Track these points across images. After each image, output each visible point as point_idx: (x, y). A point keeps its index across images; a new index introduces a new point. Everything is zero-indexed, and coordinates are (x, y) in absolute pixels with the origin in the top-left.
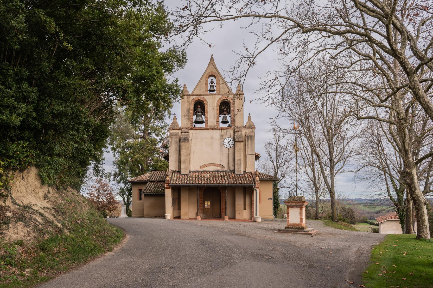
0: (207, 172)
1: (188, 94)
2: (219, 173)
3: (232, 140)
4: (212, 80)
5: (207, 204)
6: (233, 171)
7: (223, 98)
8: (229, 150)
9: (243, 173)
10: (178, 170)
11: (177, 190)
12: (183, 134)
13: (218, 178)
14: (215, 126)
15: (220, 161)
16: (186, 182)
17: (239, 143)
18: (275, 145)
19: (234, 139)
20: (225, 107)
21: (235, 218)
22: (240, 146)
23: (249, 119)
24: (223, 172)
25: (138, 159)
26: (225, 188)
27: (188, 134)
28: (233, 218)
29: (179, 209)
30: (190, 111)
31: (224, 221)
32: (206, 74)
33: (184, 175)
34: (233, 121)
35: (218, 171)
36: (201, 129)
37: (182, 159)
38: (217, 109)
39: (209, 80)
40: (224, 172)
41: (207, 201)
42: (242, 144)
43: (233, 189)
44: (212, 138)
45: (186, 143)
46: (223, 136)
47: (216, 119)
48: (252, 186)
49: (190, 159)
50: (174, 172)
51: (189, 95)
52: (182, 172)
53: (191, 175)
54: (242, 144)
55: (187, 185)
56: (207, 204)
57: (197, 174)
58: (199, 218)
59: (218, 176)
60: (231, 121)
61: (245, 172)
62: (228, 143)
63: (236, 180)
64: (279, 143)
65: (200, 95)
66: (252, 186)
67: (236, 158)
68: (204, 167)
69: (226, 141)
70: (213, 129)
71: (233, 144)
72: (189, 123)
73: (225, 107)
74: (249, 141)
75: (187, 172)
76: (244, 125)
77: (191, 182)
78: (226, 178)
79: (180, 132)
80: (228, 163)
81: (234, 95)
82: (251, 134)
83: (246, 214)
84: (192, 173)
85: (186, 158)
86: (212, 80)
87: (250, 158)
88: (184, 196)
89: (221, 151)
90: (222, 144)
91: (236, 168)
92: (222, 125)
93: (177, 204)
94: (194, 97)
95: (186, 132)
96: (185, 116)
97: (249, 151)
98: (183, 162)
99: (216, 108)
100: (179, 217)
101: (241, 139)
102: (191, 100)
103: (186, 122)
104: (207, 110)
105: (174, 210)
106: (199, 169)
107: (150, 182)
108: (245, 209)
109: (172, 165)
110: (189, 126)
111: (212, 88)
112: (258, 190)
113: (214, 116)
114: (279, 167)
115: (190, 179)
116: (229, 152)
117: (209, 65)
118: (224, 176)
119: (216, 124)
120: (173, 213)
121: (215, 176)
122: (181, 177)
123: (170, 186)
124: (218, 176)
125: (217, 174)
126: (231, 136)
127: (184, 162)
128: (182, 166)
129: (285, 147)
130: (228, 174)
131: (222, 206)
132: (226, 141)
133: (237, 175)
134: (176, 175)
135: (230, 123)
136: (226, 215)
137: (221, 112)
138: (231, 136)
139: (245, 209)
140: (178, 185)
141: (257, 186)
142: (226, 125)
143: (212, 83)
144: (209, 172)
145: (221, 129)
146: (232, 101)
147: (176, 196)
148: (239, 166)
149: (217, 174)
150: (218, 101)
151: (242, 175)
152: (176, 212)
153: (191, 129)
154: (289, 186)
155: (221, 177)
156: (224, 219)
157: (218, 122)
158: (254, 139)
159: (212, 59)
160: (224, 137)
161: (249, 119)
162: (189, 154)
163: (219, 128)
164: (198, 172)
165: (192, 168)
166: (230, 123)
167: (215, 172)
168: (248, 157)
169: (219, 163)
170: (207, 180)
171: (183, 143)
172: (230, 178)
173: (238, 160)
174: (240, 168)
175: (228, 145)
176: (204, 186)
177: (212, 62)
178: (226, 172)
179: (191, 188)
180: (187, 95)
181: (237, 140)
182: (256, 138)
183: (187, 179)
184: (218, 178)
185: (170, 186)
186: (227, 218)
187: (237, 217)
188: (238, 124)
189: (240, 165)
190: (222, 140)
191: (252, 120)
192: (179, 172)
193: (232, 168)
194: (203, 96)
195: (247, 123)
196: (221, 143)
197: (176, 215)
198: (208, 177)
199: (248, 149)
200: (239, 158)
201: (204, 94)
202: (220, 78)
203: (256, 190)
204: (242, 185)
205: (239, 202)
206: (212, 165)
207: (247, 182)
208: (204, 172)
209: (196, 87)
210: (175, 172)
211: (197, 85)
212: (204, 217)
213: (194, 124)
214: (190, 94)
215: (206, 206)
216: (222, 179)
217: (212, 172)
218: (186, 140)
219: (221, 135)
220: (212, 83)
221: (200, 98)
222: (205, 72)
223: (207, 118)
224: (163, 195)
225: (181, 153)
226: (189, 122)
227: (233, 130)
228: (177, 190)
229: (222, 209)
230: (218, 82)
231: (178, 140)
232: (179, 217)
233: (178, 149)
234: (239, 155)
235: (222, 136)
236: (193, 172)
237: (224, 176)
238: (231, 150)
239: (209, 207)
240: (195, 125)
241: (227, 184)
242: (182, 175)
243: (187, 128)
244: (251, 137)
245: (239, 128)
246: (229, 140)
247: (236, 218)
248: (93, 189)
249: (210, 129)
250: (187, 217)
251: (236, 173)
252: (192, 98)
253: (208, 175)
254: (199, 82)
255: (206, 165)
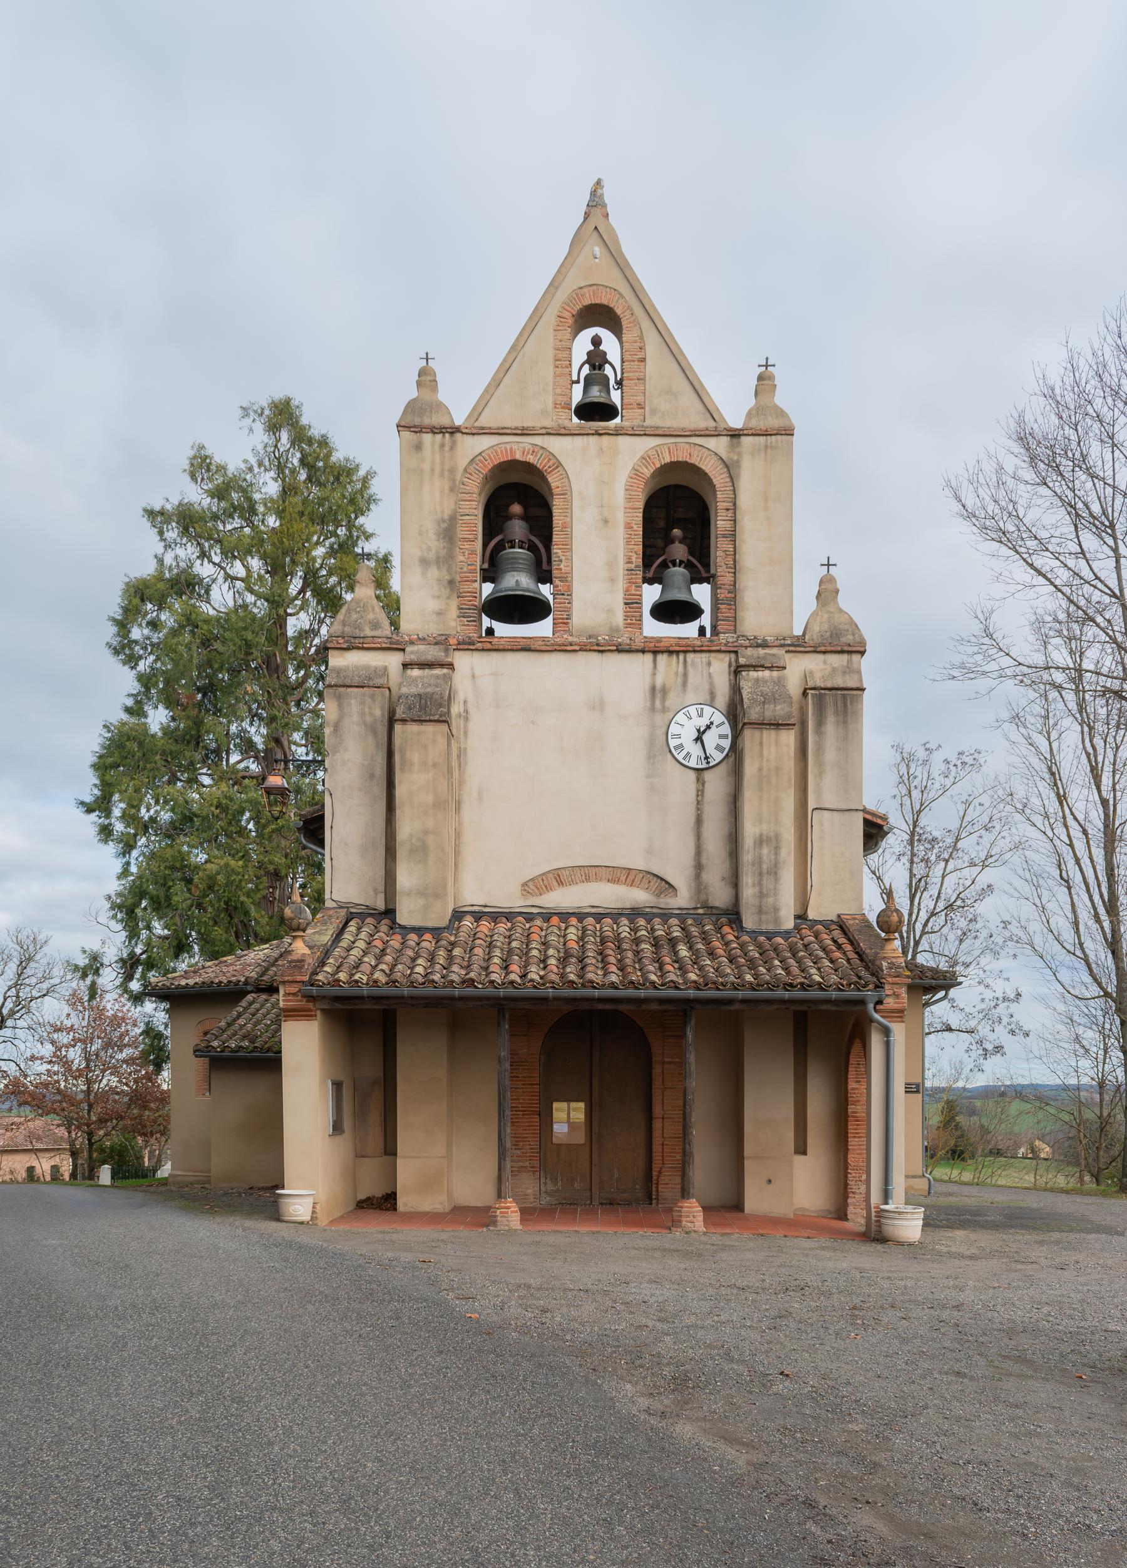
0: (564, 916)
1: (445, 422)
2: (641, 922)
3: (719, 718)
4: (596, 341)
5: (568, 1118)
6: (726, 912)
7: (668, 452)
8: (700, 781)
9: (789, 924)
10: (381, 905)
11: (370, 1026)
12: (416, 673)
13: (637, 953)
14: (614, 630)
15: (650, 852)
16: (420, 970)
17: (769, 735)
18: (905, 827)
19: (735, 714)
20: (680, 520)
21: (737, 1206)
22: (770, 752)
23: (827, 592)
24: (665, 916)
25: (221, 879)
26: (677, 1012)
27: (448, 679)
28: (729, 1206)
29: (390, 1150)
30: (461, 532)
31: (677, 1234)
32: (561, 296)
33: (419, 931)
34: (728, 603)
35: (634, 913)
36: (525, 647)
37: (406, 828)
38: (628, 526)
39: (582, 345)
40: (674, 921)
41: (569, 1100)
42: (789, 738)
43: (726, 1021)
44: (598, 705)
45: (429, 728)
46: (664, 691)
47: (621, 585)
48: (862, 1002)
49: (458, 834)
50: (352, 915)
51: (454, 430)
52: (404, 917)
53: (463, 936)
54: (789, 738)
55: (429, 990)
56: (568, 1118)
57: (502, 927)
58: (510, 1215)
59: (637, 941)
60: (715, 609)
61: (801, 917)
62: (699, 739)
63: (752, 965)
64: (922, 822)
65: (524, 432)
66: (862, 1002)
67: (750, 830)
68: (549, 888)
69: (684, 729)
70: (600, 649)
71: (726, 744)
72: (454, 612)
73: (680, 520)
74: (830, 727)
75: (439, 917)
76: (798, 631)
77: (457, 973)
78: (683, 951)
79: (392, 661)
80: (699, 867)
81: (735, 435)
82: (839, 682)
83: (805, 1184)
84: (468, 922)
85: (430, 823)
86: (596, 341)
87: (835, 837)
88: (420, 1065)
89: (652, 789)
90: (660, 747)
91: (748, 892)
92: (654, 629)
93: (375, 1117)
94: (486, 442)
95: (429, 665)
96: (424, 562)
97: (825, 789)
98: (413, 851)
99: (620, 517)
100: (386, 1202)
101: (778, 710)
102: (462, 462)
103: (433, 605)
104: (567, 527)
105: (359, 1155)
106: (514, 901)
107: (259, 990)
108: (801, 1149)
109: (347, 875)
110: (454, 625)
111: (596, 394)
112: (898, 1031)
113: (611, 565)
114: (923, 933)
115: (450, 958)
116: (700, 792)
117: (577, 241)
118: (673, 942)
119: (619, 619)
120: (352, 1177)
121: (618, 940)
122: (395, 943)
123: (310, 998)
124: (637, 941)
125: (625, 931)
126: (712, 695)
127: (420, 850)
128: (405, 878)
129: (949, 840)
130: (694, 931)
131: (657, 1134)
132: (684, 729)
133: (754, 934)
134: (366, 929)
135: (706, 620)
136: (685, 1193)
137: (653, 562)
138: (712, 695)
139: (801, 1149)
140: (365, 991)
141: (890, 1003)
142: (688, 630)
143: (597, 360)
144: (581, 917)
145: (655, 649)
146: (719, 478)
147: (372, 1068)
148: (768, 882)
149: (625, 931)
150: (636, 473)
151: (786, 935)
152: (372, 1167)
153: (466, 645)
154: (973, 1024)
155: (656, 944)
156: (674, 1223)
157: (632, 603)
158: (858, 715)
159: (596, 202)
160: (673, 700)
161: (827, 592)
162: (450, 802)
163: (639, 645)
164: (509, 916)
165: (476, 890)
166: (706, 620)
167: (616, 916)
168: (823, 826)
169: (639, 864)
170: (564, 961)
171: (413, 728)
172: (712, 954)
173: (760, 841)
174: (776, 892)
175: (696, 750)
176: (544, 1000)
177: (596, 219)
178: (682, 918)
179: (463, 1015)
180: (442, 430)
181: (753, 714)
182: (869, 702)
183: (432, 959)
184: (637, 953)
185: (310, 998)
186: (693, 1213)
187: (755, 1200)
188: (756, 618)
189: (774, 871)
190: (660, 719)
191: (844, 601)
192: (389, 913)
193: (720, 896)
194: (538, 440)
195: (814, 615)
196: (651, 741)
197: (372, 1188)
198: (573, 945)
199: (820, 774)
200: (765, 828)
201: (548, 423)
202: (646, 324)
203: (886, 1032)
204: (798, 994)
205: (768, 1102)
206: (598, 879)
207: (824, 974)
208: (547, 917)
209: (496, 382)
210: (362, 916)
211: (505, 369)
212: (546, 1200)
213: (486, 622)
214: (459, 421)
215: (560, 1129)
216: (659, 961)
217: (599, 917)
218: (433, 710)
219: (653, 689)
220: (597, 360)
221: (520, 449)
222: (554, 286)
223: (565, 594)
224: (266, 1063)
225: (400, 791)
226: (454, 603)
227: (726, 658)
228: (370, 1026)
229: (657, 1147)
230: (635, 357)
231: (379, 712)
232: (386, 1202)
233: (380, 769)
234: (767, 813)
235: (657, 693)
236: (478, 916)
237: (673, 942)
238: (717, 785)
239: (580, 1138)
240: (490, 632)
241: (696, 986)
242: (406, 930)
243: (442, 642)
244: (839, 701)
245: (765, 645)
246: (703, 723)
247: (750, 1206)
248: (64, 1038)
249: (584, 648)
250: (435, 1203)
251: (749, 922)
252: (471, 447)
253: (573, 934)
254: (516, 348)
255: (558, 878)
